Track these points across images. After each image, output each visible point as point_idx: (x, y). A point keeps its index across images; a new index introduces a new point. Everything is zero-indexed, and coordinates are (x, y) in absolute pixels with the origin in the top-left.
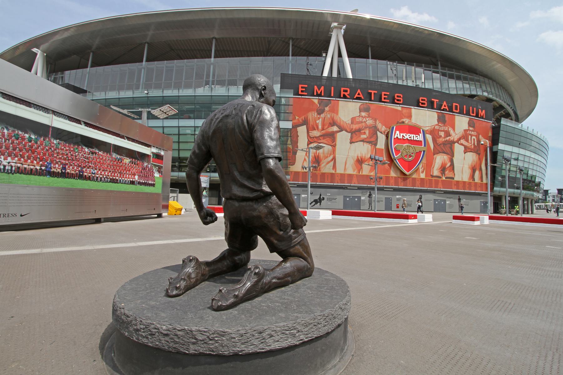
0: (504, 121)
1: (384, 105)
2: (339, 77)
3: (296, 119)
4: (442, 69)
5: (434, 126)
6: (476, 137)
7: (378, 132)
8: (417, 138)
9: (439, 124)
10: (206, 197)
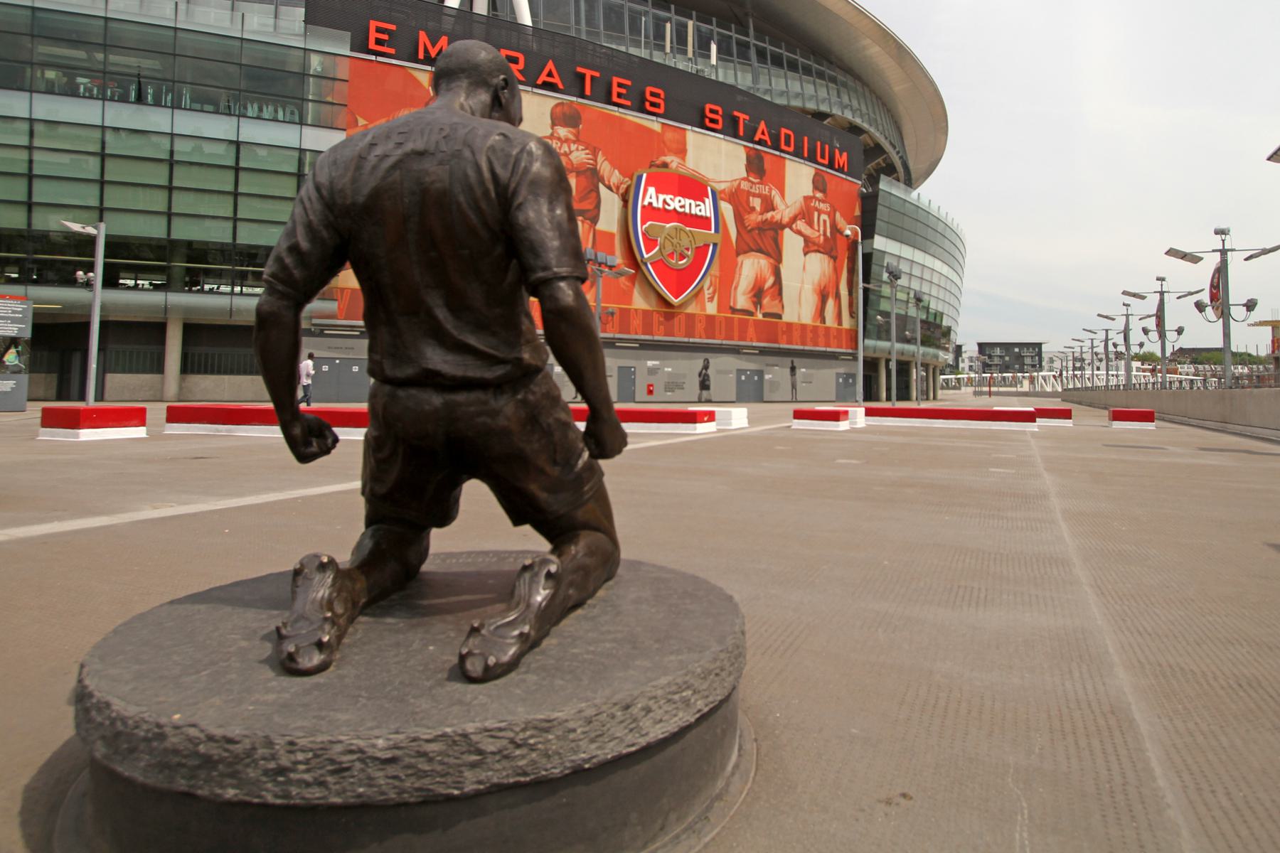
0: (885, 184)
1: (617, 114)
2: (493, 15)
3: (360, 124)
4: (757, 39)
5: (737, 182)
6: (829, 217)
7: (601, 186)
8: (699, 208)
9: (751, 179)
10: (19, 372)
